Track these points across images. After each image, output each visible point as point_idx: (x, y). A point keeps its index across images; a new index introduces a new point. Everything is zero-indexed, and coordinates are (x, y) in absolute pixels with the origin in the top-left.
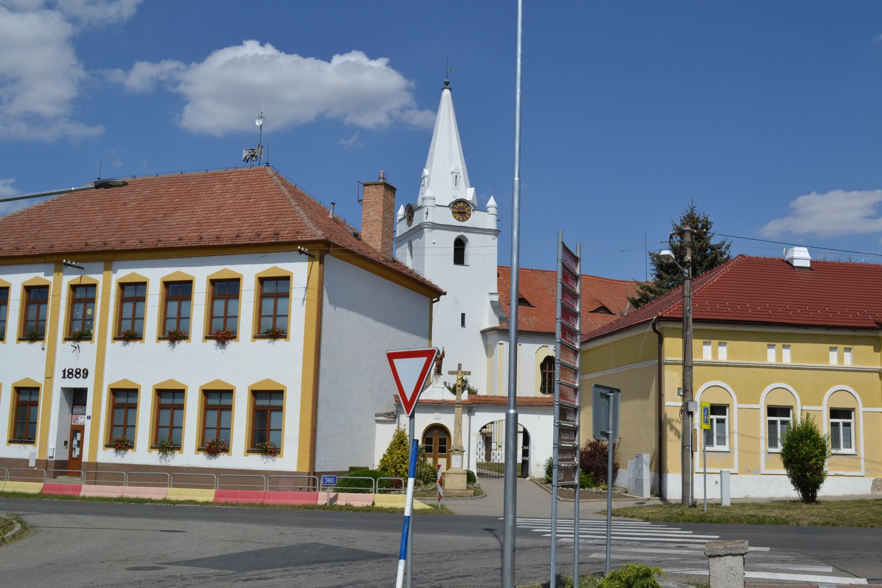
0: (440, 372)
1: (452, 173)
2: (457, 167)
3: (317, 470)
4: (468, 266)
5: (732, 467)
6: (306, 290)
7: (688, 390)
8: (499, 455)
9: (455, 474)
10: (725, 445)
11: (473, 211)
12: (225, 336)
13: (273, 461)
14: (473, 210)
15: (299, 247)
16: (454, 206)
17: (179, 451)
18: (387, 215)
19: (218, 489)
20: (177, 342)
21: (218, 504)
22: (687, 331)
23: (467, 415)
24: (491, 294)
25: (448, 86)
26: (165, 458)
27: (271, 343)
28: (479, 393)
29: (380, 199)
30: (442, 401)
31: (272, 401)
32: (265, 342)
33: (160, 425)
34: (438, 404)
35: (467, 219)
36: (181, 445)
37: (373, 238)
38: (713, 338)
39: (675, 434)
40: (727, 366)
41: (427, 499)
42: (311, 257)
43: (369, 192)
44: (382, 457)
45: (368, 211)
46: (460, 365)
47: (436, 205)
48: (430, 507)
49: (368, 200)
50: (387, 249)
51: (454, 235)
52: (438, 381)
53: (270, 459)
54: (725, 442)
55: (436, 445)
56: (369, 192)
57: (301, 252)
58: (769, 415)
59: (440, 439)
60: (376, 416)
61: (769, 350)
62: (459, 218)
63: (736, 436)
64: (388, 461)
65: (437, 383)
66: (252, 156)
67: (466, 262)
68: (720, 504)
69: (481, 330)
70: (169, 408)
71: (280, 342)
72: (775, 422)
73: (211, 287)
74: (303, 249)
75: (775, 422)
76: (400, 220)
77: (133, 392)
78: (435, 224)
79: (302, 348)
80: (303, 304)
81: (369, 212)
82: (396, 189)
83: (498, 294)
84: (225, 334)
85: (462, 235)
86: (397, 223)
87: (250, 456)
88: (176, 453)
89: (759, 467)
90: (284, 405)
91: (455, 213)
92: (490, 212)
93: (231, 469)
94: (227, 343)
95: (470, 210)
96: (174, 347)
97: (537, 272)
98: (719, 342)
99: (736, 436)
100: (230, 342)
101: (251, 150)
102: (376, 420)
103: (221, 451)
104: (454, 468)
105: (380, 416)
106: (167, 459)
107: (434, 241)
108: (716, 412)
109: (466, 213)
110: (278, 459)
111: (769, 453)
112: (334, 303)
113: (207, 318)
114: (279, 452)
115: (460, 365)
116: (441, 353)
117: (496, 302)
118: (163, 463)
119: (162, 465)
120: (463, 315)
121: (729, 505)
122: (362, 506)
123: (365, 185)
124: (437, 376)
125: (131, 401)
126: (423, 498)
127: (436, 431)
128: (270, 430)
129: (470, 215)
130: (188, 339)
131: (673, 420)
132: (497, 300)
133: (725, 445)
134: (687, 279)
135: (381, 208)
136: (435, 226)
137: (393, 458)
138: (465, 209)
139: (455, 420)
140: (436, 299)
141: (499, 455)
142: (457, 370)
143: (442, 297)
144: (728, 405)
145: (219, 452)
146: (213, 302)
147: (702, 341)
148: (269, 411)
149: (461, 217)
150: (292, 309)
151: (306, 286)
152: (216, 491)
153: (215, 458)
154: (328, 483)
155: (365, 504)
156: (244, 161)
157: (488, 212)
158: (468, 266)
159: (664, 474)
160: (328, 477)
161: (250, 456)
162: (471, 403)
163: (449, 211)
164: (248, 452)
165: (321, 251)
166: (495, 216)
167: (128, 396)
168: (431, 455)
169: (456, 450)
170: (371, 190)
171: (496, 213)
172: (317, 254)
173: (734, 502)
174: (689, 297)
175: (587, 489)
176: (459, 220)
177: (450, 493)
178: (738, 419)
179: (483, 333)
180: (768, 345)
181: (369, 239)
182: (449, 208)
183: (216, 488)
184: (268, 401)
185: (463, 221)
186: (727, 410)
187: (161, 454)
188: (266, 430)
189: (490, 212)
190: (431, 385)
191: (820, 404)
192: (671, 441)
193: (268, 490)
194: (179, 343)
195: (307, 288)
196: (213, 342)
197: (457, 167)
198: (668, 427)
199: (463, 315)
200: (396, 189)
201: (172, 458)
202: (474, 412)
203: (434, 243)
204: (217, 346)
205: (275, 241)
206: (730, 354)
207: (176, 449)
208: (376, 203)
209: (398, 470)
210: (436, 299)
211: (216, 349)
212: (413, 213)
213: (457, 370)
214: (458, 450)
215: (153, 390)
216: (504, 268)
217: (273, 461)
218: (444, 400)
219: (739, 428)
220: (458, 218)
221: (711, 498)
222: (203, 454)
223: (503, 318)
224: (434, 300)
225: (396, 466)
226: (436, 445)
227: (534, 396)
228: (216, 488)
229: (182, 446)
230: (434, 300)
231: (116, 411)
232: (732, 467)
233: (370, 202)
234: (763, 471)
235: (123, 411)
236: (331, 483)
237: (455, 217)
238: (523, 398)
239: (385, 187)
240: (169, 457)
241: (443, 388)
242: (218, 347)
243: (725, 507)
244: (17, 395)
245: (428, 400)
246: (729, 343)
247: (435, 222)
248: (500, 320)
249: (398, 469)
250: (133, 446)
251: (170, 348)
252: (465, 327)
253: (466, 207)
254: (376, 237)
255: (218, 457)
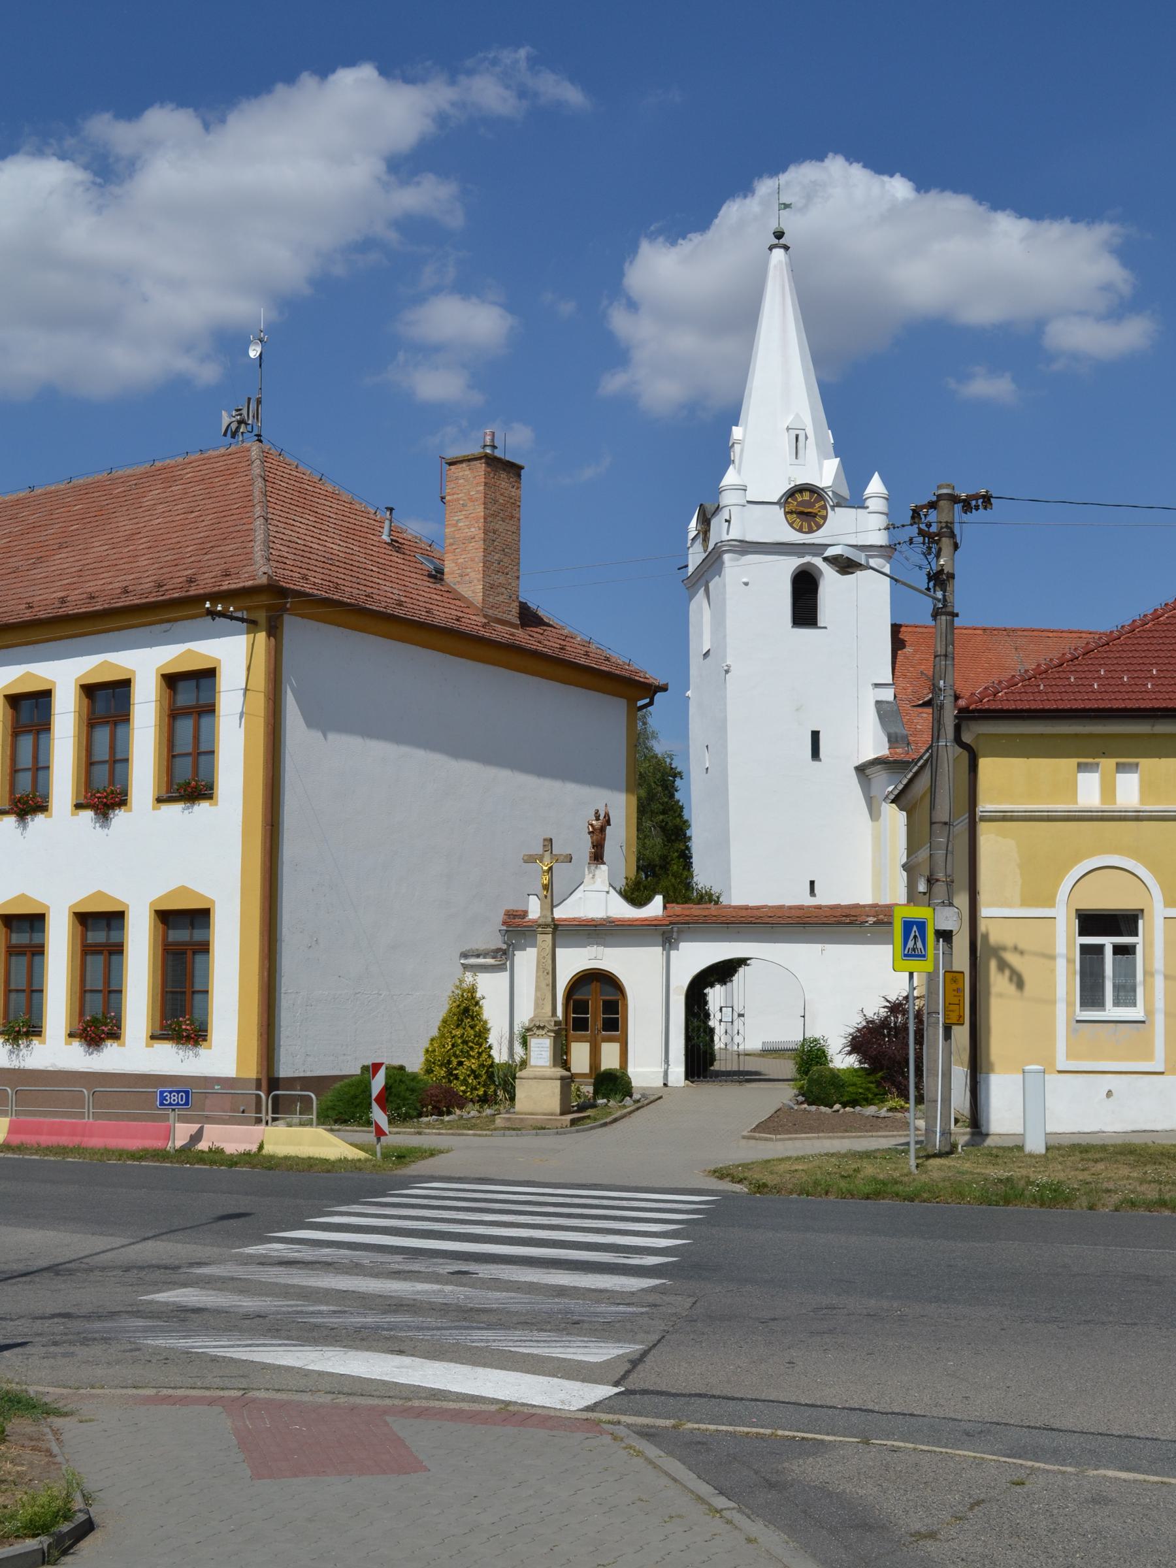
0: (602, 859)
1: (788, 429)
2: (797, 415)
3: (285, 1071)
4: (825, 628)
5: (1149, 1056)
6: (245, 694)
7: (937, 880)
8: (738, 1033)
9: (535, 1078)
10: (1135, 1006)
11: (833, 510)
12: (105, 800)
13: (196, 1055)
14: (833, 507)
15: (208, 605)
16: (790, 500)
17: (39, 1038)
18: (500, 526)
19: (14, 1118)
20: (29, 817)
21: (19, 1149)
22: (938, 738)
23: (661, 948)
24: (877, 685)
25: (782, 241)
26: (16, 1053)
27: (186, 812)
28: (724, 900)
29: (478, 492)
30: (604, 920)
31: (196, 931)
32: (176, 809)
33: (34, 988)
34: (596, 926)
35: (819, 527)
36: (42, 1027)
37: (467, 577)
38: (1104, 755)
39: (1011, 979)
40: (1137, 819)
41: (467, 1135)
42: (252, 625)
43: (457, 478)
44: (427, 1044)
45: (456, 518)
46: (549, 842)
47: (749, 502)
48: (361, 1155)
49: (455, 496)
50: (501, 598)
51: (790, 565)
52: (596, 877)
53: (191, 1052)
54: (1135, 999)
55: (595, 1016)
56: (457, 478)
57: (212, 614)
58: (1082, 933)
59: (606, 1003)
60: (465, 955)
61: (1082, 777)
62: (801, 527)
63: (1159, 982)
64: (434, 1051)
65: (594, 882)
66: (240, 422)
67: (821, 621)
68: (1020, 1148)
69: (857, 764)
70: (100, 953)
71: (203, 807)
72: (1100, 949)
73: (86, 701)
74: (219, 608)
75: (1100, 949)
76: (693, 539)
77: (115, 919)
78: (747, 542)
79: (240, 818)
80: (240, 724)
81: (458, 521)
82: (521, 468)
83: (893, 684)
84: (106, 797)
85: (809, 563)
86: (689, 548)
87: (73, 1043)
88: (34, 1042)
89: (1054, 1058)
90: (125, 941)
91: (791, 512)
92: (871, 509)
93: (124, 1074)
94: (112, 816)
95: (824, 507)
96: (25, 828)
97: (996, 632)
98: (1117, 764)
99: (1159, 982)
100: (117, 812)
101: (237, 410)
102: (462, 964)
103: (108, 1038)
104: (535, 1066)
105: (478, 956)
106: (21, 1055)
107: (745, 580)
108: (1123, 928)
109: (814, 515)
110: (202, 1051)
111: (1078, 1021)
112: (317, 720)
113: (79, 766)
114: (204, 1038)
115: (549, 842)
116: (601, 818)
117: (888, 702)
118: (14, 1064)
119: (12, 1067)
120: (815, 735)
121: (1043, 1151)
122: (236, 1153)
123: (451, 464)
124: (593, 867)
125: (198, 935)
126: (461, 1132)
127: (595, 986)
128: (194, 992)
129: (825, 518)
130: (47, 810)
131: (1004, 949)
132: (891, 698)
133: (1135, 1006)
134: (942, 614)
135: (480, 510)
136: (746, 547)
137: (444, 1047)
138: (812, 505)
139: (538, 962)
140: (647, 701)
141: (738, 1033)
142: (541, 852)
143: (659, 697)
144: (1142, 910)
145: (103, 1040)
146: (115, 732)
147: (1075, 761)
148: (189, 953)
149: (805, 525)
150: (221, 738)
151: (244, 687)
152: (11, 1121)
153: (98, 1051)
154: (170, 1104)
155: (242, 1147)
156: (225, 434)
157: (867, 507)
158: (825, 628)
159: (983, 1076)
160: (170, 1092)
161: (155, 1045)
162: (668, 923)
163: (779, 512)
164: (153, 1037)
165: (269, 608)
166: (884, 517)
167: (109, 927)
168: (584, 1036)
169: (539, 1027)
170: (461, 474)
171: (885, 510)
172: (261, 616)
173: (1054, 1142)
174: (946, 656)
175: (858, 1108)
176: (800, 530)
177: (522, 1120)
178: (1166, 943)
179: (861, 770)
180: (1079, 765)
181: (459, 579)
182: (777, 507)
183: (12, 1115)
184: (28, 935)
185: (811, 531)
186: (1140, 922)
187: (9, 1047)
188: (185, 992)
189: (871, 509)
190: (581, 887)
191: (1050, 902)
192: (1000, 995)
193: (91, 1120)
194: (33, 820)
195: (246, 690)
196: (88, 814)
197: (797, 415)
198: (993, 964)
199: (815, 735)
200: (521, 468)
201: (29, 1053)
202: (678, 941)
203: (746, 584)
204: (96, 822)
205: (183, 594)
206: (1146, 789)
207: (33, 1035)
208: (471, 500)
209: (455, 1072)
210: (647, 701)
211: (94, 828)
212: (709, 524)
213: (541, 852)
214: (543, 1028)
215: (150, 911)
216: (918, 630)
217: (196, 1055)
218: (608, 917)
219: (1166, 965)
220: (797, 525)
221: (1096, 1129)
222: (78, 1043)
223: (897, 737)
224: (640, 703)
225: (449, 1062)
226: (595, 1016)
227: (870, 902)
228: (12, 1115)
229: (43, 1030)
230: (640, 703)
231: (89, 958)
232: (1149, 1056)
233: (458, 499)
234: (1062, 1063)
235: (24, 960)
236: (178, 1104)
237: (791, 525)
238: (790, 908)
239: (487, 463)
240: (24, 1051)
241: (608, 892)
242: (98, 825)
243: (1031, 1156)
244: (82, 931)
245: (574, 919)
246: (1144, 762)
247: (747, 539)
248: (889, 741)
249: (456, 1069)
250: (41, 1031)
251: (19, 831)
252: (820, 760)
253: (816, 501)
254: (472, 575)
255: (102, 1049)
